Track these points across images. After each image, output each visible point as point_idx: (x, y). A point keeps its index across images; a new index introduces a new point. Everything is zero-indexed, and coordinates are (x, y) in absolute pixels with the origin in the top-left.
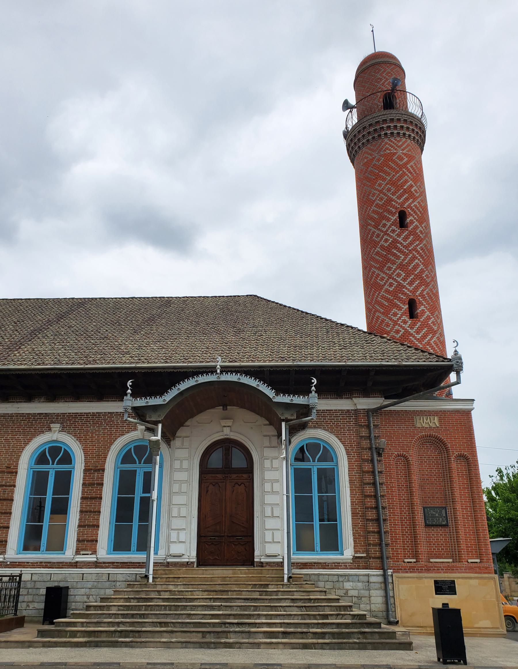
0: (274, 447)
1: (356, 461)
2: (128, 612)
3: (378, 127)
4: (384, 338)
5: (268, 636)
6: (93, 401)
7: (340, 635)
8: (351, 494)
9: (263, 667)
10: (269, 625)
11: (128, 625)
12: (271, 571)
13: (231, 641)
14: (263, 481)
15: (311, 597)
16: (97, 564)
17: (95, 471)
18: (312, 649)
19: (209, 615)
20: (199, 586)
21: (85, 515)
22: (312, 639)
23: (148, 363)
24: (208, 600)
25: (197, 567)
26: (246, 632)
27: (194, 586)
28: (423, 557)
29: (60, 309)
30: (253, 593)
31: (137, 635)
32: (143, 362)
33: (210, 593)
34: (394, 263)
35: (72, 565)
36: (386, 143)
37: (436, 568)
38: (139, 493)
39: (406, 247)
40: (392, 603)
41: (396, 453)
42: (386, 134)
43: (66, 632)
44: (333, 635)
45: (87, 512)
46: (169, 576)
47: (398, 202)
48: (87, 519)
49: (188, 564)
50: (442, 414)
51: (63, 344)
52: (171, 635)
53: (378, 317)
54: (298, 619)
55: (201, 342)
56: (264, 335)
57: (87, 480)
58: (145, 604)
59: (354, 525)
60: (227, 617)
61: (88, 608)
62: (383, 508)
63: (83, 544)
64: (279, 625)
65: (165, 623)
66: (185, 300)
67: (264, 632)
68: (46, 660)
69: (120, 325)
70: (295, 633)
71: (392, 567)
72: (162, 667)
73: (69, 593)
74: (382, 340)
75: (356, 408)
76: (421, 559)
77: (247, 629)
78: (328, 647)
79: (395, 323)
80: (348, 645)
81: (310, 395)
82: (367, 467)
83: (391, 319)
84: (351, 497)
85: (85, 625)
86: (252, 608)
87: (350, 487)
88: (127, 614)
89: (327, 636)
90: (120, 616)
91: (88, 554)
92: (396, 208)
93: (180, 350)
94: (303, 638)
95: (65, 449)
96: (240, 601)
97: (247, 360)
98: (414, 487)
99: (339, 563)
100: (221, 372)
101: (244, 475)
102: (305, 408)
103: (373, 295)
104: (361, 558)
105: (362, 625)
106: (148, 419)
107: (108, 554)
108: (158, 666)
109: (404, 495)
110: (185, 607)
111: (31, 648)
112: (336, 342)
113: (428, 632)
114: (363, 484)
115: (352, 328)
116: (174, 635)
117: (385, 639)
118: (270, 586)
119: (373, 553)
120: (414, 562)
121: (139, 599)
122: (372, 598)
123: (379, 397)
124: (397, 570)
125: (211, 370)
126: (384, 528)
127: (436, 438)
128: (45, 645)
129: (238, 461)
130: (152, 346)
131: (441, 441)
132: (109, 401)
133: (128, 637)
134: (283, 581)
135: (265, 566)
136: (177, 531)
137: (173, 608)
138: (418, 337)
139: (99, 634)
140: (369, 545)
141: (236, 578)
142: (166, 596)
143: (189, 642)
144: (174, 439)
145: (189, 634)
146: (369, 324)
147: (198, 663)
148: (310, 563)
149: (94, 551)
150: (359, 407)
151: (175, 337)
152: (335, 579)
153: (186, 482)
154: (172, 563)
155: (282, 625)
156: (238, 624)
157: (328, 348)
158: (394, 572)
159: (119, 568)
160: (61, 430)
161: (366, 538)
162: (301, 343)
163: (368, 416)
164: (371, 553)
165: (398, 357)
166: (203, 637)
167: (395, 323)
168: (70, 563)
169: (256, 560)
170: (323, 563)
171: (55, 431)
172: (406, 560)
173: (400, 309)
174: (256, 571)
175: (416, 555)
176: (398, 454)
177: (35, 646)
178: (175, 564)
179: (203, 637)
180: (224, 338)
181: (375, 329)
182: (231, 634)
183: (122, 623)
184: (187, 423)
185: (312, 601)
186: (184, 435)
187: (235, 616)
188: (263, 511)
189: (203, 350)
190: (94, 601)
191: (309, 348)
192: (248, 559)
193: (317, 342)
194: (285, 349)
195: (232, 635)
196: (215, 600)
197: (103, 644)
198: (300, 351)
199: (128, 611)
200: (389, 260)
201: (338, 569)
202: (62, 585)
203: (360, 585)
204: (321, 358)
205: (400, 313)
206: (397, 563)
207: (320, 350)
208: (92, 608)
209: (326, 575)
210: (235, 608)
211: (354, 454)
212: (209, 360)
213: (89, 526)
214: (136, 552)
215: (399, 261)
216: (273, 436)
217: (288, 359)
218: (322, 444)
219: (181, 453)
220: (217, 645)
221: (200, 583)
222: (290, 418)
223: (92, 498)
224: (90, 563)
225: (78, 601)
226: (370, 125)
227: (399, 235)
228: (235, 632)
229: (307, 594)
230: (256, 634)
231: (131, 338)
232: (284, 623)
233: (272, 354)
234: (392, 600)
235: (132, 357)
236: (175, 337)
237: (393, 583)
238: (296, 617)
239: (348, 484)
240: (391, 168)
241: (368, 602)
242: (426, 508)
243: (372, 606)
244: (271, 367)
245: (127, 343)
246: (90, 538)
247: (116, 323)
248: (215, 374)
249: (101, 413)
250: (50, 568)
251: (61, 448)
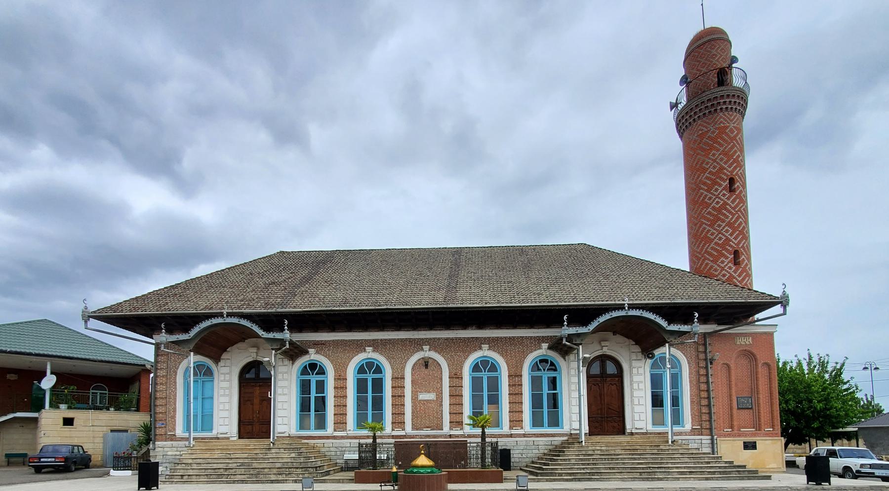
3: (715, 102)
7: (724, 473)
10: (677, 468)
16: (524, 435)
34: (723, 221)
36: (721, 117)
37: (745, 435)
38: (313, 394)
39: (734, 208)
42: (721, 109)
47: (728, 170)
50: (753, 335)
59: (692, 409)
79: (723, 269)
83: (719, 266)
92: (727, 175)
103: (703, 246)
124: (720, 436)
125: (221, 315)
127: (749, 351)
129: (611, 369)
131: (752, 354)
136: (575, 412)
138: (740, 279)
142: (599, 452)
173: (727, 258)
188: (632, 401)
192: (621, 430)
200: (719, 219)
205: (727, 261)
215: (728, 220)
220: (653, 479)
226: (709, 100)
227: (728, 199)
240: (724, 140)
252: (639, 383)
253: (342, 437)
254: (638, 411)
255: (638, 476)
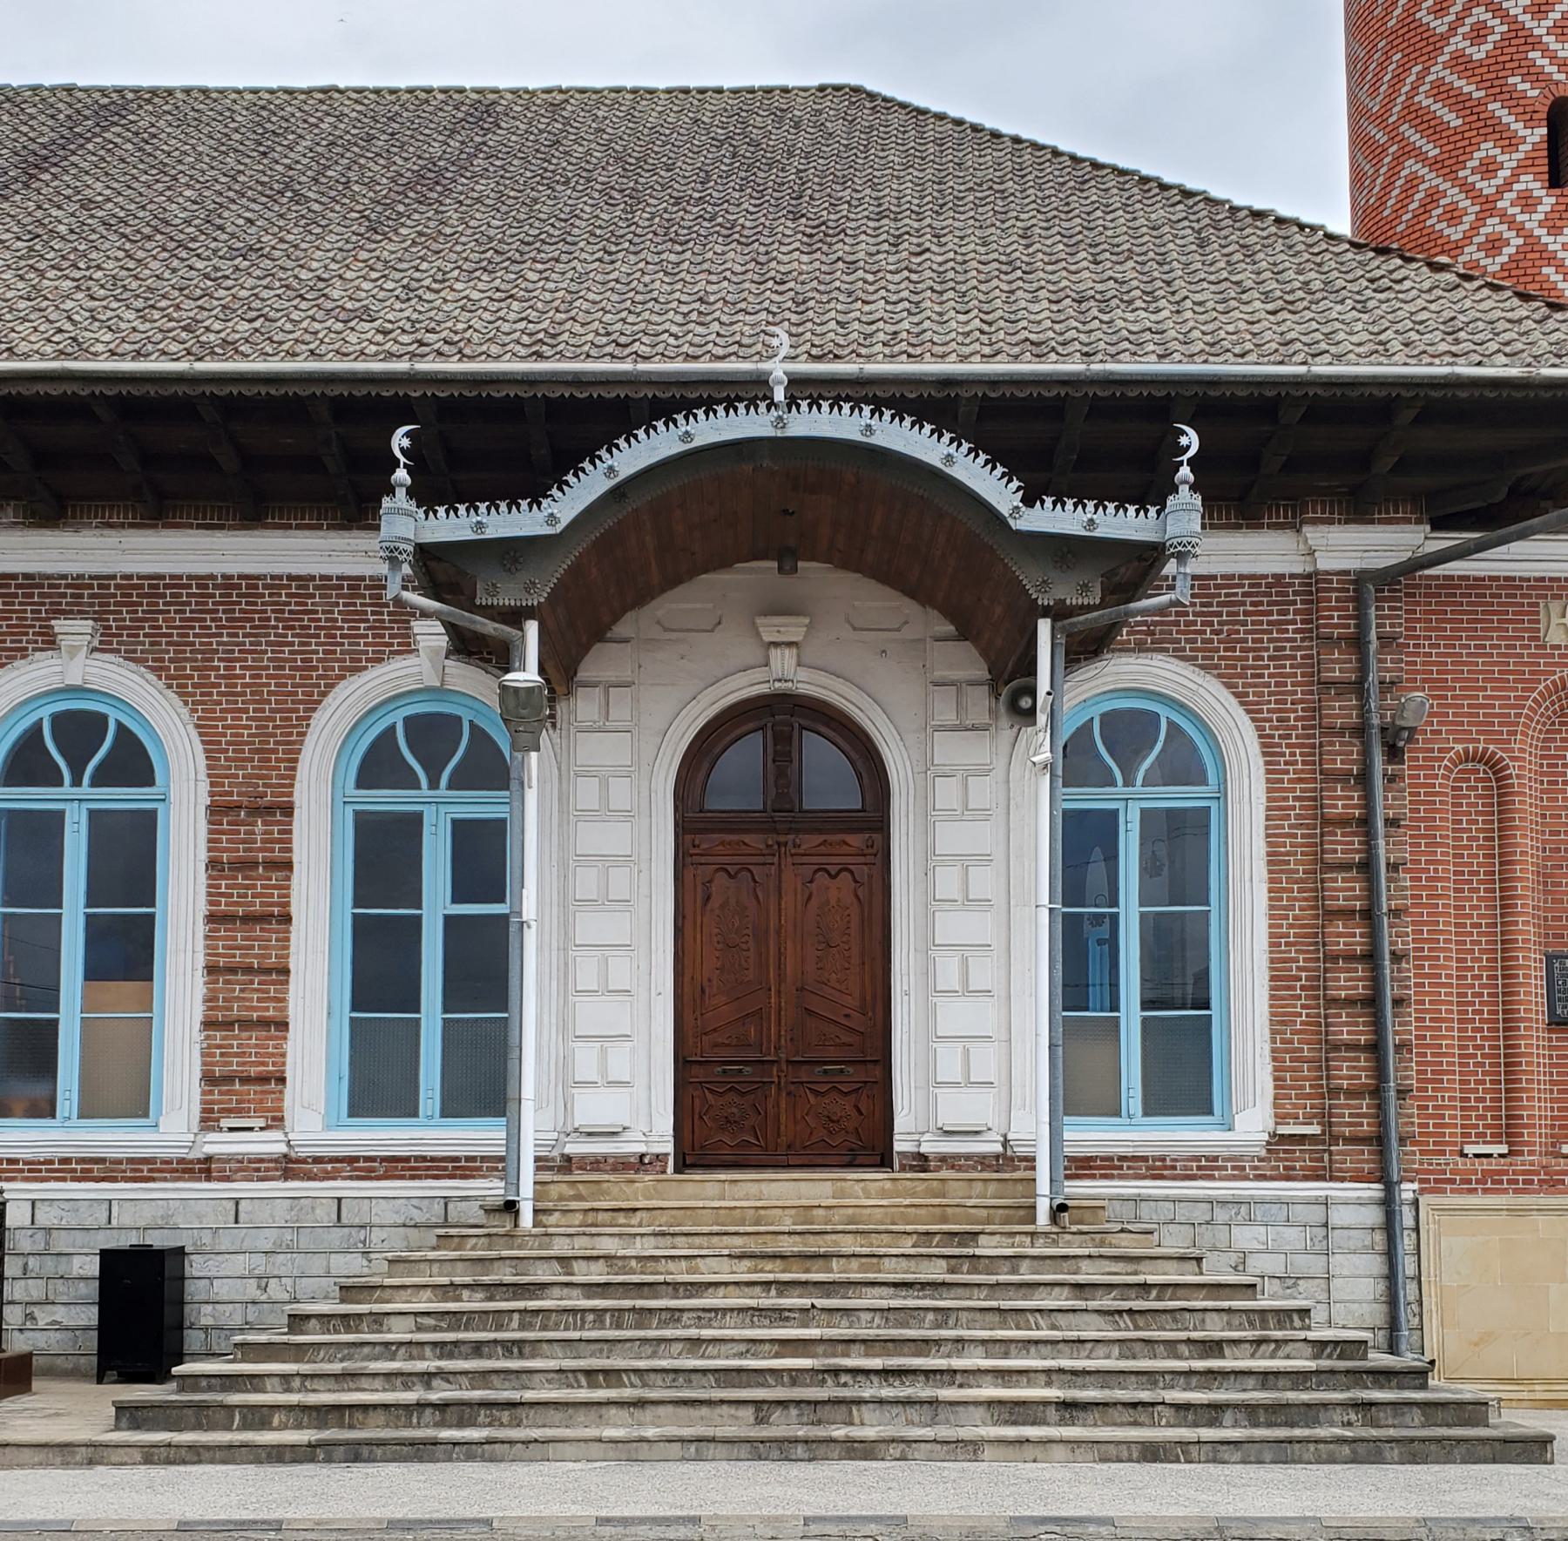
0: (974, 728)
1: (1300, 780)
2: (462, 1336)
4: (1442, 268)
5: (1007, 1416)
6: (221, 527)
7: (1277, 1413)
8: (1271, 907)
9: (1043, 1529)
10: (1003, 1376)
11: (464, 1381)
12: (979, 1186)
13: (870, 1433)
14: (929, 858)
15: (1151, 1279)
16: (288, 1167)
17: (255, 811)
18: (1178, 1461)
19: (772, 1341)
20: (715, 1239)
21: (227, 982)
22: (1169, 1425)
23: (463, 357)
24: (758, 1289)
25: (677, 1170)
26: (922, 1403)
27: (697, 1240)
28: (1536, 1136)
29: (24, 129)
30: (925, 1263)
31: (505, 1416)
32: (440, 353)
33: (761, 1264)
35: (191, 1171)
38: (437, 899)
40: (1411, 1298)
41: (1459, 747)
43: (230, 1408)
44: (1251, 1412)
45: (232, 970)
46: (596, 1205)
48: (238, 999)
49: (641, 1163)
51: (78, 274)
52: (637, 1413)
53: (1413, 182)
54: (1108, 1357)
55: (666, 274)
56: (934, 248)
57: (225, 850)
58: (520, 1304)
59: (1279, 1022)
60: (840, 1348)
61: (297, 1322)
62: (1397, 957)
63: (228, 1093)
64: (1043, 1378)
65: (606, 1372)
66: (556, 101)
67: (990, 1403)
68: (192, 1514)
69: (298, 198)
70: (1106, 1404)
71: (1417, 1171)
72: (658, 1531)
73: (188, 1271)
74: (1437, 276)
75: (1309, 569)
76: (1527, 1144)
77: (925, 1392)
78: (1238, 1456)
80: (1312, 1447)
81: (1171, 501)
82: (1343, 802)
83: (1468, 189)
84: (1271, 917)
85: (296, 1383)
86: (931, 1316)
87: (1271, 881)
88: (456, 1343)
89: (1228, 1417)
90: (428, 1351)
91: (250, 1129)
93: (586, 306)
94: (1135, 1424)
95: (120, 725)
96: (876, 1291)
97: (887, 351)
98: (1520, 879)
99: (1216, 1159)
100: (792, 402)
101: (850, 838)
102: (1140, 559)
103: (1398, 79)
104: (1302, 1139)
105: (1357, 1377)
106: (482, 599)
107: (327, 1127)
108: (642, 1530)
109: (1478, 907)
110: (674, 1315)
111: (100, 1468)
112: (1249, 284)
113: (1538, 1396)
114: (1322, 865)
115: (1302, 227)
116: (649, 1413)
117: (1449, 1426)
118: (982, 1239)
119: (1349, 1124)
120: (1501, 1156)
121: (492, 1290)
122: (1335, 1283)
123: (1408, 521)
124: (1436, 1183)
125: (751, 391)
126: (1396, 1033)
128: (151, 1455)
129: (825, 776)
130: (459, 286)
132: (289, 527)
133: (473, 1424)
134: (1033, 1221)
135: (938, 1169)
136: (600, 1035)
137: (629, 1318)
139: (359, 1415)
140: (1334, 1092)
141: (850, 1211)
143: (713, 1440)
144: (568, 693)
145: (704, 1411)
146: (1363, 213)
147: (796, 1517)
148: (1103, 1159)
149: (274, 1119)
150: (1325, 563)
151: (551, 251)
152: (1200, 1213)
153: (626, 860)
154: (583, 1158)
155: (1054, 1377)
156: (885, 1373)
157: (1220, 307)
158: (1422, 1191)
159: (378, 1178)
160: (96, 643)
161: (1323, 1067)
162: (1099, 287)
163: (1360, 601)
164: (1340, 1124)
165: (1520, 346)
166: (760, 1421)
167: (1488, 206)
168: (181, 1161)
169: (898, 1147)
170: (1155, 1159)
171: (73, 651)
172: (1470, 1150)
173: (1510, 142)
174: (921, 1187)
175: (1509, 1131)
176: (1466, 751)
177: (114, 1459)
178: (596, 1163)
179: (760, 1421)
180: (762, 259)
181: (1384, 235)
182: (864, 1408)
183: (440, 1373)
184: (620, 629)
185: (1154, 1293)
186: (609, 675)
187: (869, 1345)
188: (928, 972)
189: (685, 309)
190: (286, 1297)
191: (1139, 303)
192: (869, 1143)
193: (1168, 283)
194: (1036, 308)
195: (867, 1412)
196: (784, 1287)
197: (379, 1452)
198: (1106, 318)
199: (458, 1329)
201: (1211, 1178)
202: (157, 1240)
203: (1293, 1236)
204: (1201, 346)
205: (1509, 161)
206: (1435, 1159)
207: (1189, 314)
208: (313, 1321)
209: (1166, 1199)
210: (866, 1316)
211: (1293, 754)
212: (720, 352)
213: (246, 1024)
214: (437, 1120)
216: (972, 683)
217: (1060, 349)
218: (1164, 713)
219: (595, 749)
221: (716, 1228)
222: (1073, 600)
223: (249, 919)
224: (261, 1161)
225: (226, 1298)
228: (882, 1402)
229: (1130, 1267)
230: (960, 1409)
231: (363, 255)
232: (1061, 1371)
233: (986, 328)
234: (1411, 1288)
235: (385, 333)
236: (551, 251)
237: (1417, 1230)
238: (1101, 1350)
239: (1261, 870)
241: (1323, 1297)
242: (1557, 957)
243: (1335, 1308)
244: (994, 382)
245: (349, 275)
246: (253, 1071)
247: (281, 193)
248: (762, 406)
249: (258, 577)
250: (103, 1179)
251: (103, 719)
252: (967, 861)
253: (254, 1168)
254: (973, 1033)
255: (739, 1425)
